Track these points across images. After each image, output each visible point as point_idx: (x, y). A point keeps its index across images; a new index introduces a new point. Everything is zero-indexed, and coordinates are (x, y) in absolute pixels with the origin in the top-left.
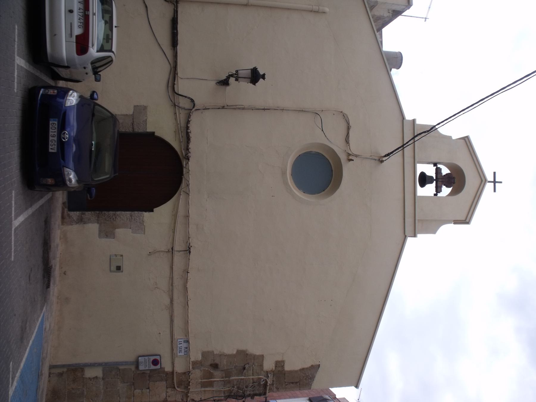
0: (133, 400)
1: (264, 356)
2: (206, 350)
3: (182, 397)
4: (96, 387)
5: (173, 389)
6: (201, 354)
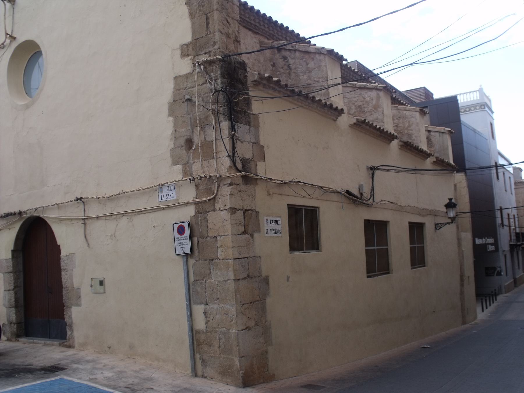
0: (231, 259)
1: (174, 76)
2: (169, 160)
3: (226, 186)
4: (216, 314)
5: (217, 201)
6: (175, 166)
